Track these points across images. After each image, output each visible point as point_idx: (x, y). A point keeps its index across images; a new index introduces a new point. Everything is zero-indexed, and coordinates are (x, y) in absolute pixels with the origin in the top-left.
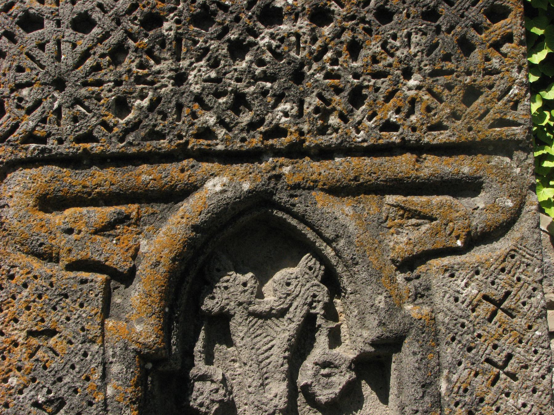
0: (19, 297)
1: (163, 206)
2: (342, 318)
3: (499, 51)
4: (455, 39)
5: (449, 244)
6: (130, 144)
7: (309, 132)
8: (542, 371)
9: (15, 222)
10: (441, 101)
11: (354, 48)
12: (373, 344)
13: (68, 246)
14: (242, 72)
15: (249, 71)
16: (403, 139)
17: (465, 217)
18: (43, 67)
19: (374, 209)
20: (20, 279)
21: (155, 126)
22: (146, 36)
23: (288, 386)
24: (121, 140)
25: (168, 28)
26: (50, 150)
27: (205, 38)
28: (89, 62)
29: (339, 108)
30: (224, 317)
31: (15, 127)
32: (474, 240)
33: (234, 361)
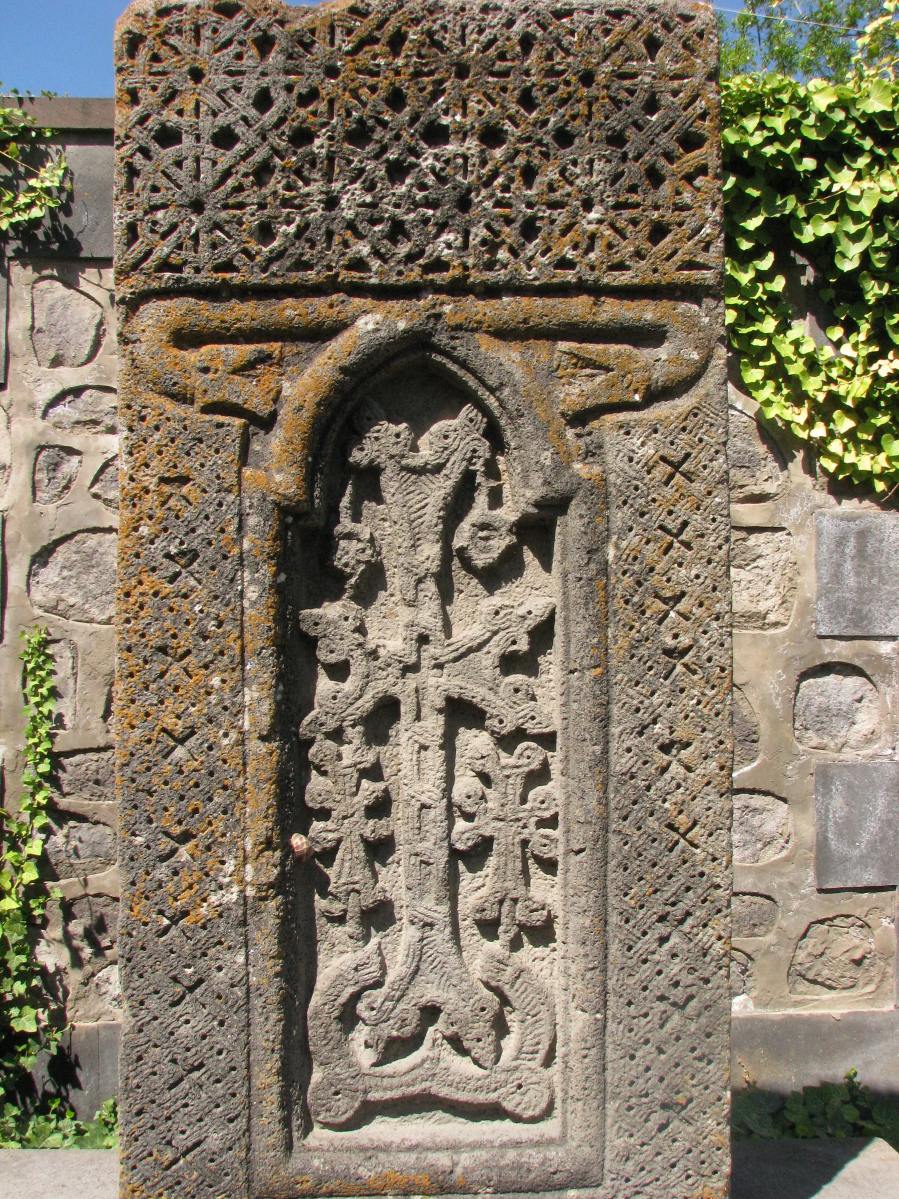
0: (150, 440)
1: (309, 345)
2: (505, 477)
3: (691, 184)
4: (642, 169)
5: (626, 398)
6: (274, 275)
7: (474, 266)
8: (719, 541)
9: (147, 358)
10: (624, 238)
11: (529, 174)
12: (536, 504)
13: (204, 387)
14: (401, 197)
15: (409, 196)
16: (580, 278)
17: (646, 368)
18: (179, 187)
19: (544, 356)
20: (151, 421)
21: (302, 255)
22: (295, 153)
23: (442, 548)
24: (264, 270)
25: (319, 145)
26: (186, 280)
27: (360, 157)
28: (231, 182)
29: (509, 241)
30: (373, 472)
31: (148, 254)
32: (656, 395)
33: (384, 520)
